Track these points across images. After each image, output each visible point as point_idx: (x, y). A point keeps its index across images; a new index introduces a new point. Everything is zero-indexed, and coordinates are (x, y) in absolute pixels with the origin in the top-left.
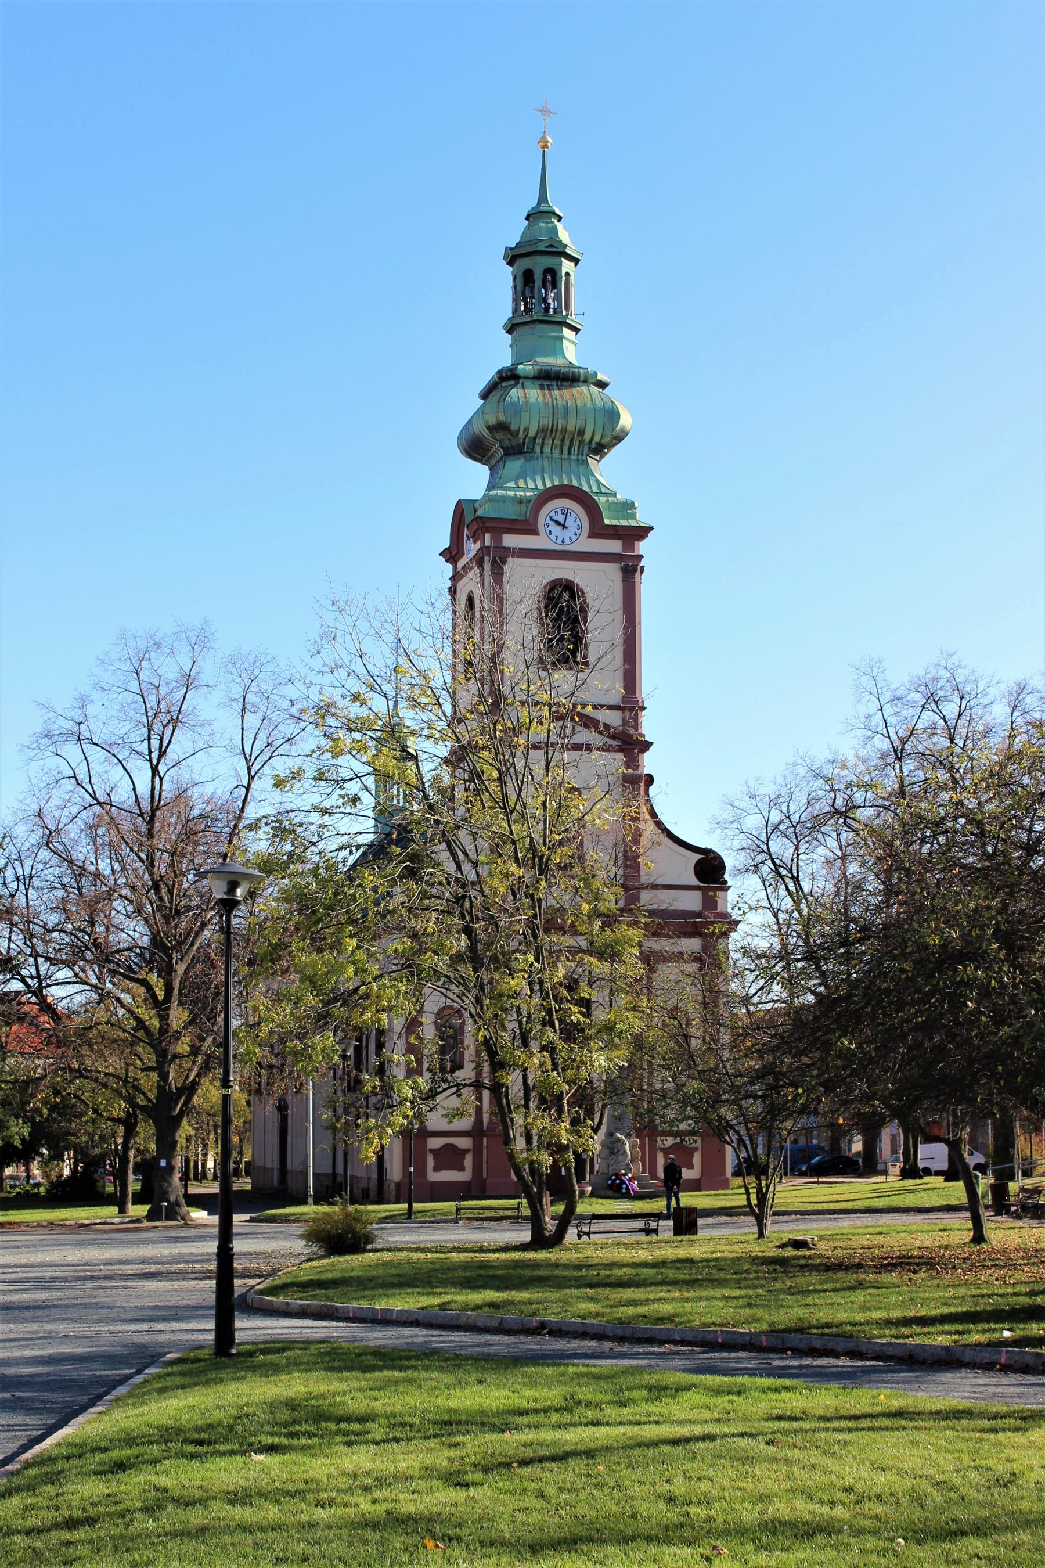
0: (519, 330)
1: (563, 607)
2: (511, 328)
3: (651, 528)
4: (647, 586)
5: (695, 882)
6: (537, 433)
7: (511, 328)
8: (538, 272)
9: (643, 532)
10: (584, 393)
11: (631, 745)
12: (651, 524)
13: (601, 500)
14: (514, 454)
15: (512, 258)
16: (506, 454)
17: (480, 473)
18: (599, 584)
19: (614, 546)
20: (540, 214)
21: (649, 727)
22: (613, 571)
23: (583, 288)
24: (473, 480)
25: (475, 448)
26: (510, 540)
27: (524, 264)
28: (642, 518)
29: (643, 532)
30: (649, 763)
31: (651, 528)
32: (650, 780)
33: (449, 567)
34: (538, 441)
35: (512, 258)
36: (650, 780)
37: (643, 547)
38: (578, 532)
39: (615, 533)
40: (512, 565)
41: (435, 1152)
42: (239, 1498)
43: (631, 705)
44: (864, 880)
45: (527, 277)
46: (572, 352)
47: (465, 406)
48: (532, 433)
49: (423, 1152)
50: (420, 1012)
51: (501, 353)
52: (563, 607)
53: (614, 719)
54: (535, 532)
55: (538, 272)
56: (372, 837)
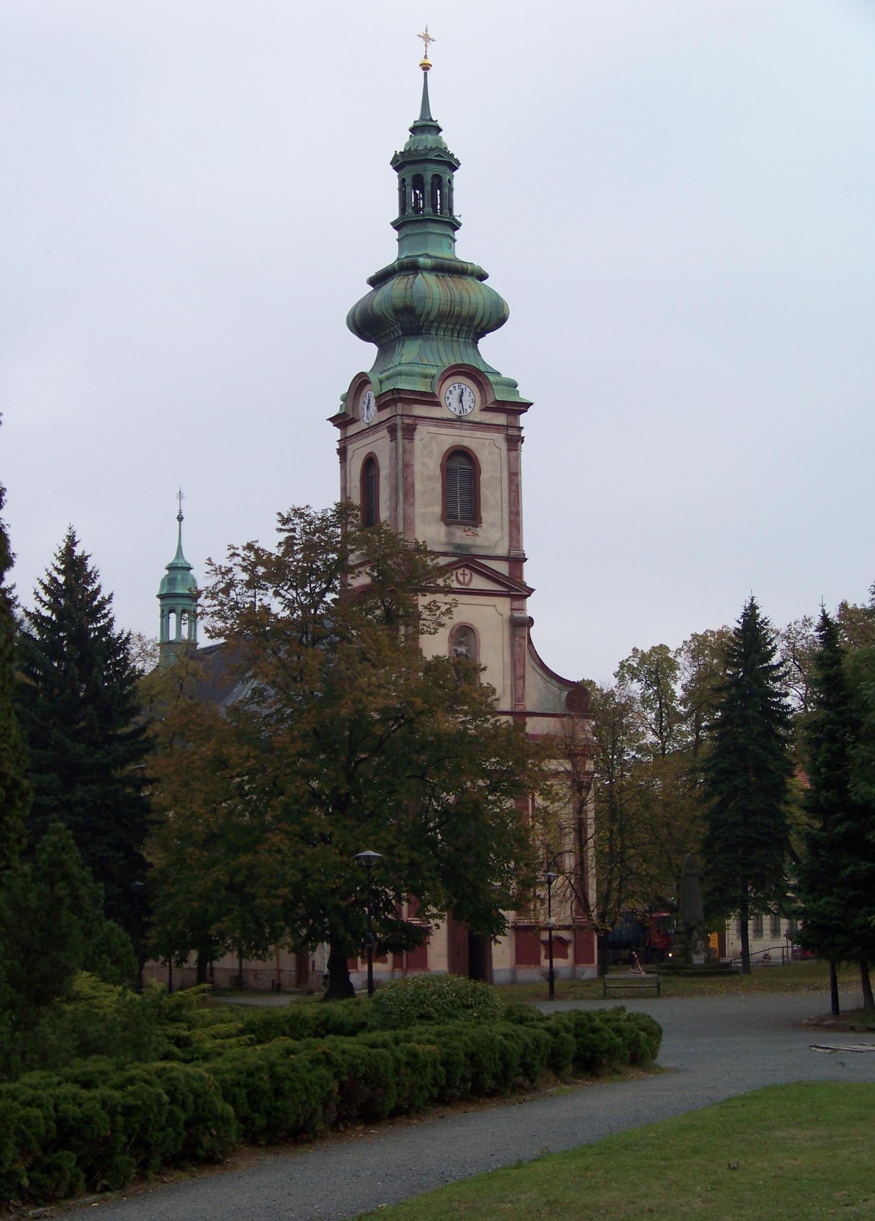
0: (408, 230)
1: (460, 466)
2: (398, 225)
3: (531, 404)
4: (525, 448)
5: (567, 712)
6: (436, 317)
7: (398, 225)
8: (425, 175)
10: (467, 288)
11: (516, 590)
12: (530, 400)
13: (491, 378)
14: (412, 334)
16: (404, 335)
17: (371, 350)
18: (488, 450)
19: (500, 419)
20: (426, 127)
22: (499, 438)
23: (466, 194)
24: (365, 355)
26: (419, 410)
27: (410, 172)
28: (524, 395)
30: (532, 607)
31: (531, 404)
32: (530, 622)
33: (337, 433)
34: (435, 325)
35: (400, 163)
36: (530, 622)
38: (472, 405)
39: (501, 407)
40: (423, 432)
43: (517, 561)
44: (28, 793)
45: (418, 182)
46: (466, 248)
48: (432, 318)
51: (387, 251)
52: (460, 466)
53: (502, 568)
54: (438, 404)
55: (425, 175)
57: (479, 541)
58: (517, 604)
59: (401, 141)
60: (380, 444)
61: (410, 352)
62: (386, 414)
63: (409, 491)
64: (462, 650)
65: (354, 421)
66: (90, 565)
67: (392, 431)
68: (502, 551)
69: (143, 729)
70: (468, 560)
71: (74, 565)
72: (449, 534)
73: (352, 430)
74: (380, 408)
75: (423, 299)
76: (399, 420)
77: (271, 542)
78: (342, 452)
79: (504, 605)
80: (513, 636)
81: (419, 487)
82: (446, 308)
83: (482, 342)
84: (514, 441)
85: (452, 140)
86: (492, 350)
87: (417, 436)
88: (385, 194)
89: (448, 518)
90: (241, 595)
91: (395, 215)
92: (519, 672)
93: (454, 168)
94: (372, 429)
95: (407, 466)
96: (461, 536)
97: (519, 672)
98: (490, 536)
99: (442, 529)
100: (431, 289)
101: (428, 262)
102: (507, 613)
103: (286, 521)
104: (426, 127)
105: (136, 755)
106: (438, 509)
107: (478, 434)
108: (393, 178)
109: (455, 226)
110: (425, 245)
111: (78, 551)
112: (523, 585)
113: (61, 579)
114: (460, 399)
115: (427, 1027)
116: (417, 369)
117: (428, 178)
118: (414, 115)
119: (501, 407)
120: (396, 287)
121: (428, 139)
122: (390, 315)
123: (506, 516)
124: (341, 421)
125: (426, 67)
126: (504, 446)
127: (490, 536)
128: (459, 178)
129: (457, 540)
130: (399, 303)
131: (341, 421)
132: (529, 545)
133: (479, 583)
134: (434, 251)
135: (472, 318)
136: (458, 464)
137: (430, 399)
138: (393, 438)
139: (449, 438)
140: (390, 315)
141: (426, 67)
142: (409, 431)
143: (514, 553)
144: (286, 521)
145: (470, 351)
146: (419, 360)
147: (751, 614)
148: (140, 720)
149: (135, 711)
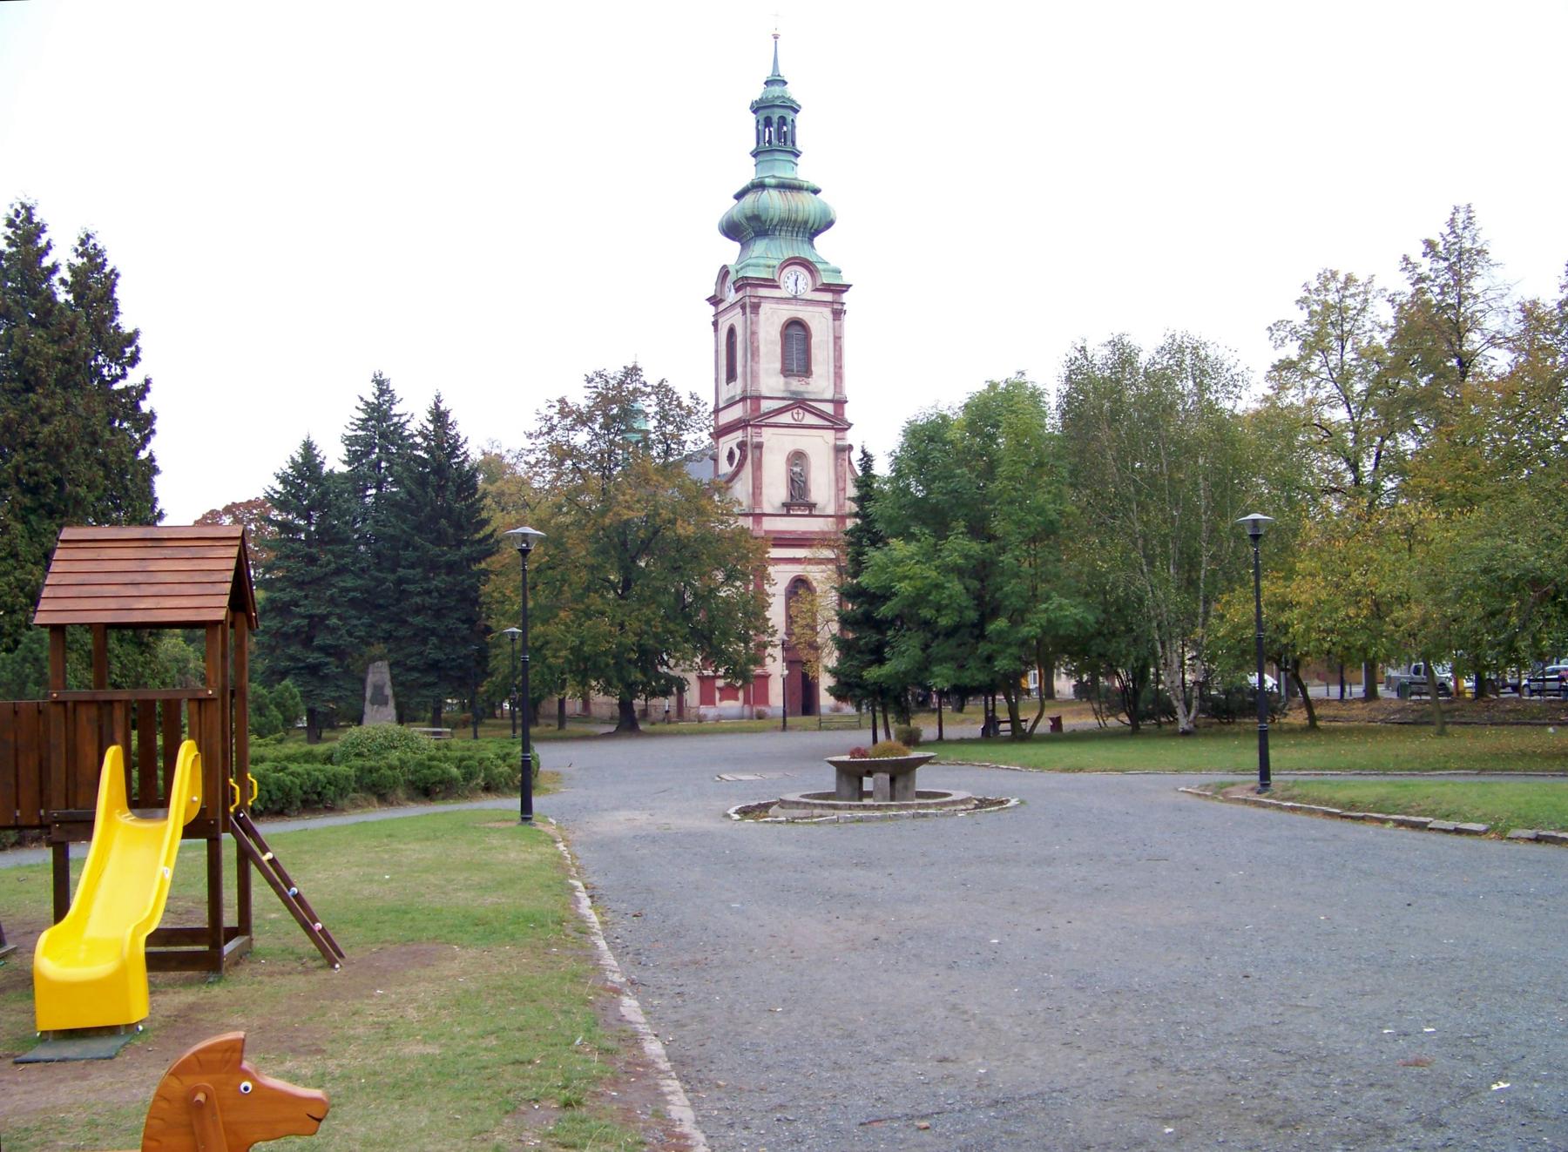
0: (761, 158)
1: (796, 332)
2: (755, 154)
4: (847, 320)
8: (775, 122)
9: (845, 288)
13: (819, 266)
15: (757, 108)
17: (736, 246)
18: (818, 321)
19: (828, 297)
20: (775, 81)
21: (850, 413)
22: (827, 312)
23: (805, 130)
25: (732, 230)
26: (763, 292)
27: (763, 114)
29: (845, 288)
33: (712, 310)
35: (757, 108)
37: (845, 297)
39: (827, 288)
40: (765, 308)
41: (720, 689)
42: (1335, 719)
43: (839, 403)
45: (768, 122)
46: (804, 171)
47: (725, 206)
49: (713, 687)
50: (433, 632)
51: (747, 172)
52: (796, 332)
53: (829, 408)
54: (778, 287)
55: (775, 122)
56: (67, 533)
57: (810, 388)
58: (840, 435)
59: (757, 92)
60: (735, 318)
61: (760, 247)
62: (740, 295)
63: (754, 352)
64: (797, 469)
65: (722, 301)
66: (1100, 354)
67: (743, 307)
68: (829, 395)
69: (491, 535)
70: (800, 403)
71: (439, 416)
72: (786, 383)
73: (722, 307)
74: (737, 290)
75: (766, 210)
76: (747, 300)
77: (580, 398)
78: (715, 324)
79: (829, 436)
80: (836, 458)
81: (763, 349)
82: (785, 215)
83: (817, 240)
84: (838, 314)
85: (793, 91)
87: (762, 310)
88: (746, 129)
89: (786, 371)
90: (558, 434)
92: (841, 485)
93: (796, 111)
94: (733, 305)
95: (753, 333)
96: (796, 384)
97: (841, 485)
98: (819, 385)
99: (782, 379)
100: (774, 203)
101: (773, 181)
102: (832, 442)
103: (590, 380)
104: (775, 81)
105: (489, 553)
106: (778, 365)
107: (810, 308)
108: (751, 119)
110: (772, 168)
111: (442, 408)
112: (844, 421)
113: (431, 427)
114: (795, 282)
116: (762, 261)
117: (775, 119)
118: (767, 73)
119: (827, 288)
120: (749, 199)
121: (776, 90)
122: (744, 221)
123: (832, 369)
124: (715, 301)
125: (776, 37)
126: (830, 317)
127: (819, 385)
128: (800, 119)
129: (793, 388)
130: (749, 213)
131: (715, 301)
132: (849, 390)
133: (810, 419)
134: (784, 172)
135: (806, 222)
136: (795, 331)
137: (771, 284)
138: (744, 313)
139: (788, 312)
140: (744, 221)
141: (776, 37)
142: (756, 308)
143: (837, 397)
144: (590, 380)
145: (806, 246)
146: (768, 253)
148: (488, 530)
149: (485, 522)
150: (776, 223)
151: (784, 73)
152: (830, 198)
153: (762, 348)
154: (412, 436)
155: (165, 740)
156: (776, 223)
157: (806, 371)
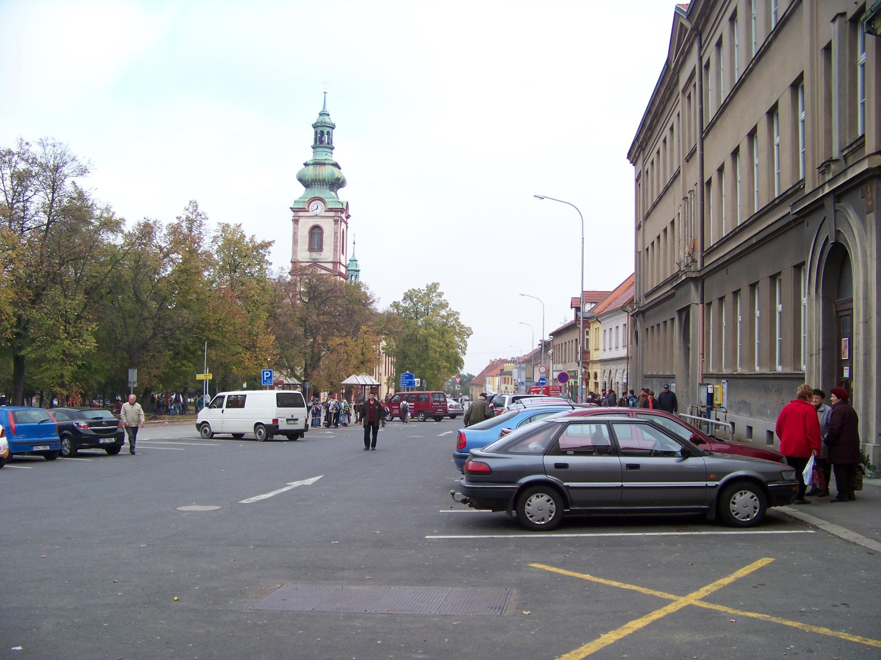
8: (323, 135)
18: (328, 226)
19: (332, 214)
23: (337, 136)
46: (336, 157)
51: (309, 156)
53: (330, 266)
55: (323, 135)
59: (315, 118)
68: (331, 259)
85: (333, 119)
86: (343, 194)
87: (300, 223)
88: (310, 137)
89: (311, 249)
91: (312, 143)
93: (333, 128)
96: (315, 255)
99: (308, 253)
106: (307, 247)
108: (313, 131)
109: (332, 148)
115: (458, 426)
118: (320, 110)
121: (326, 118)
126: (333, 223)
128: (335, 133)
136: (316, 231)
147: (266, 245)
150: (322, 182)
151: (329, 110)
152: (345, 173)
153: (299, 240)
154: (481, 381)
155: (839, 487)
156: (322, 182)
157: (320, 249)
